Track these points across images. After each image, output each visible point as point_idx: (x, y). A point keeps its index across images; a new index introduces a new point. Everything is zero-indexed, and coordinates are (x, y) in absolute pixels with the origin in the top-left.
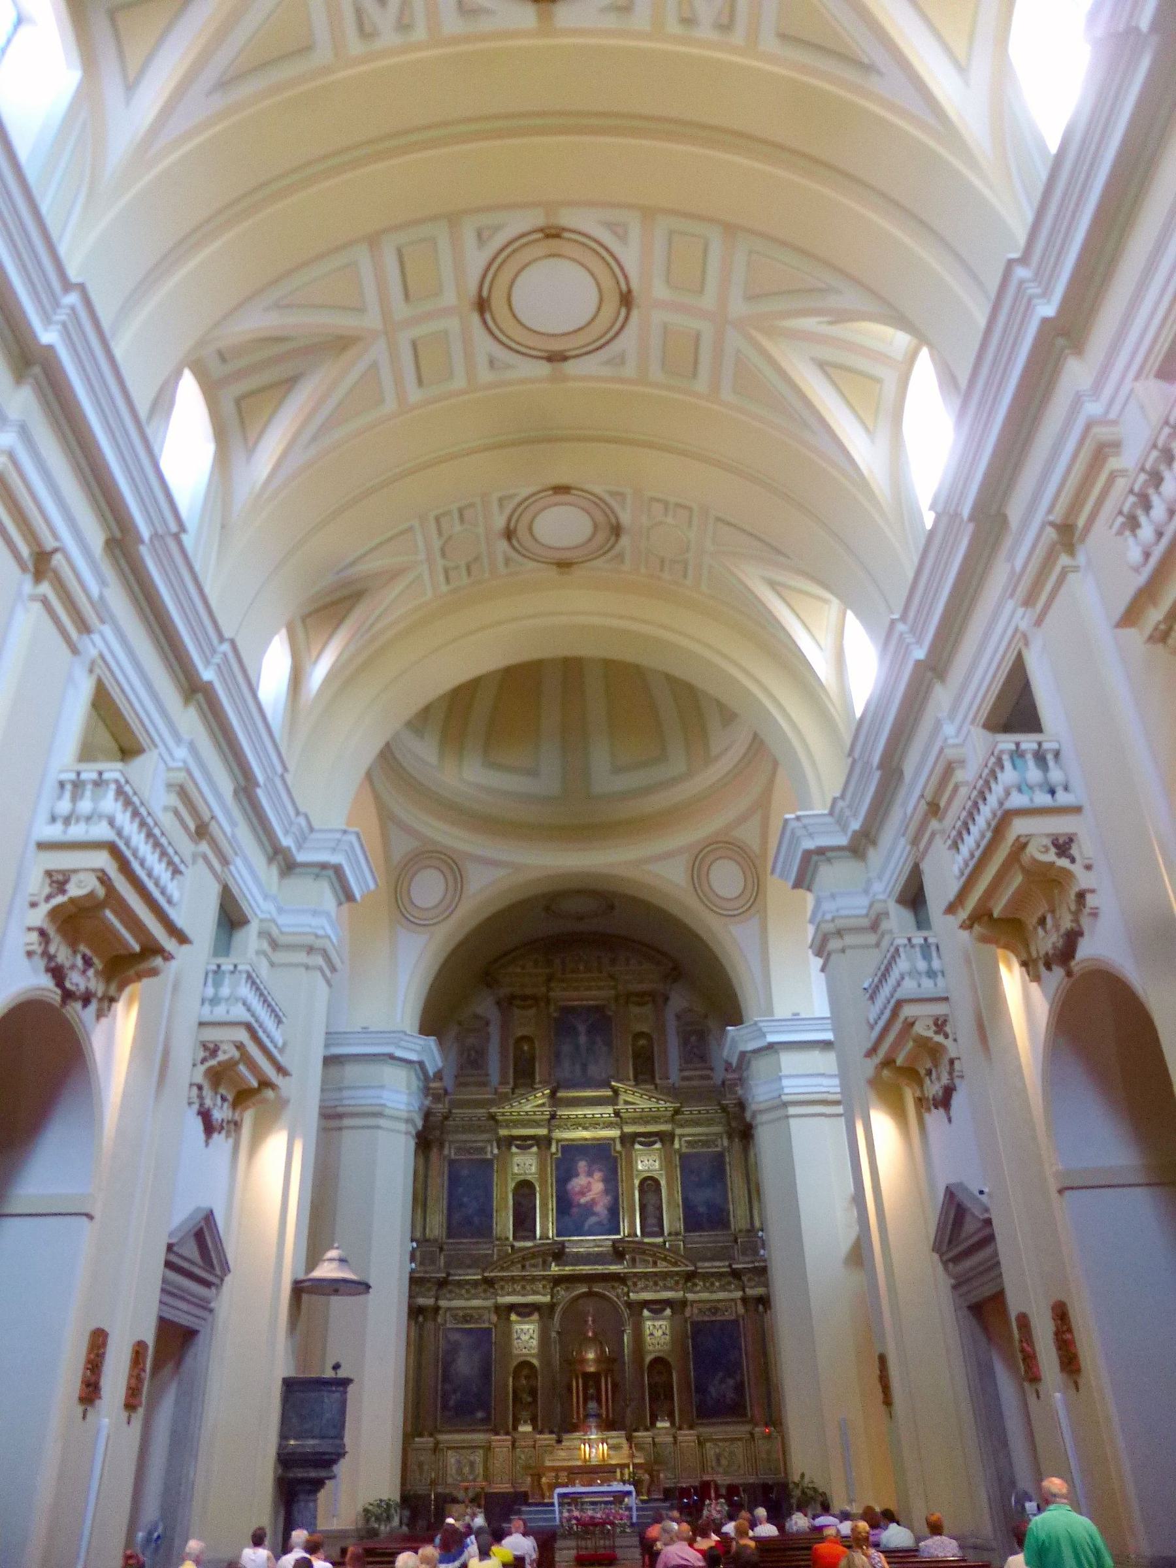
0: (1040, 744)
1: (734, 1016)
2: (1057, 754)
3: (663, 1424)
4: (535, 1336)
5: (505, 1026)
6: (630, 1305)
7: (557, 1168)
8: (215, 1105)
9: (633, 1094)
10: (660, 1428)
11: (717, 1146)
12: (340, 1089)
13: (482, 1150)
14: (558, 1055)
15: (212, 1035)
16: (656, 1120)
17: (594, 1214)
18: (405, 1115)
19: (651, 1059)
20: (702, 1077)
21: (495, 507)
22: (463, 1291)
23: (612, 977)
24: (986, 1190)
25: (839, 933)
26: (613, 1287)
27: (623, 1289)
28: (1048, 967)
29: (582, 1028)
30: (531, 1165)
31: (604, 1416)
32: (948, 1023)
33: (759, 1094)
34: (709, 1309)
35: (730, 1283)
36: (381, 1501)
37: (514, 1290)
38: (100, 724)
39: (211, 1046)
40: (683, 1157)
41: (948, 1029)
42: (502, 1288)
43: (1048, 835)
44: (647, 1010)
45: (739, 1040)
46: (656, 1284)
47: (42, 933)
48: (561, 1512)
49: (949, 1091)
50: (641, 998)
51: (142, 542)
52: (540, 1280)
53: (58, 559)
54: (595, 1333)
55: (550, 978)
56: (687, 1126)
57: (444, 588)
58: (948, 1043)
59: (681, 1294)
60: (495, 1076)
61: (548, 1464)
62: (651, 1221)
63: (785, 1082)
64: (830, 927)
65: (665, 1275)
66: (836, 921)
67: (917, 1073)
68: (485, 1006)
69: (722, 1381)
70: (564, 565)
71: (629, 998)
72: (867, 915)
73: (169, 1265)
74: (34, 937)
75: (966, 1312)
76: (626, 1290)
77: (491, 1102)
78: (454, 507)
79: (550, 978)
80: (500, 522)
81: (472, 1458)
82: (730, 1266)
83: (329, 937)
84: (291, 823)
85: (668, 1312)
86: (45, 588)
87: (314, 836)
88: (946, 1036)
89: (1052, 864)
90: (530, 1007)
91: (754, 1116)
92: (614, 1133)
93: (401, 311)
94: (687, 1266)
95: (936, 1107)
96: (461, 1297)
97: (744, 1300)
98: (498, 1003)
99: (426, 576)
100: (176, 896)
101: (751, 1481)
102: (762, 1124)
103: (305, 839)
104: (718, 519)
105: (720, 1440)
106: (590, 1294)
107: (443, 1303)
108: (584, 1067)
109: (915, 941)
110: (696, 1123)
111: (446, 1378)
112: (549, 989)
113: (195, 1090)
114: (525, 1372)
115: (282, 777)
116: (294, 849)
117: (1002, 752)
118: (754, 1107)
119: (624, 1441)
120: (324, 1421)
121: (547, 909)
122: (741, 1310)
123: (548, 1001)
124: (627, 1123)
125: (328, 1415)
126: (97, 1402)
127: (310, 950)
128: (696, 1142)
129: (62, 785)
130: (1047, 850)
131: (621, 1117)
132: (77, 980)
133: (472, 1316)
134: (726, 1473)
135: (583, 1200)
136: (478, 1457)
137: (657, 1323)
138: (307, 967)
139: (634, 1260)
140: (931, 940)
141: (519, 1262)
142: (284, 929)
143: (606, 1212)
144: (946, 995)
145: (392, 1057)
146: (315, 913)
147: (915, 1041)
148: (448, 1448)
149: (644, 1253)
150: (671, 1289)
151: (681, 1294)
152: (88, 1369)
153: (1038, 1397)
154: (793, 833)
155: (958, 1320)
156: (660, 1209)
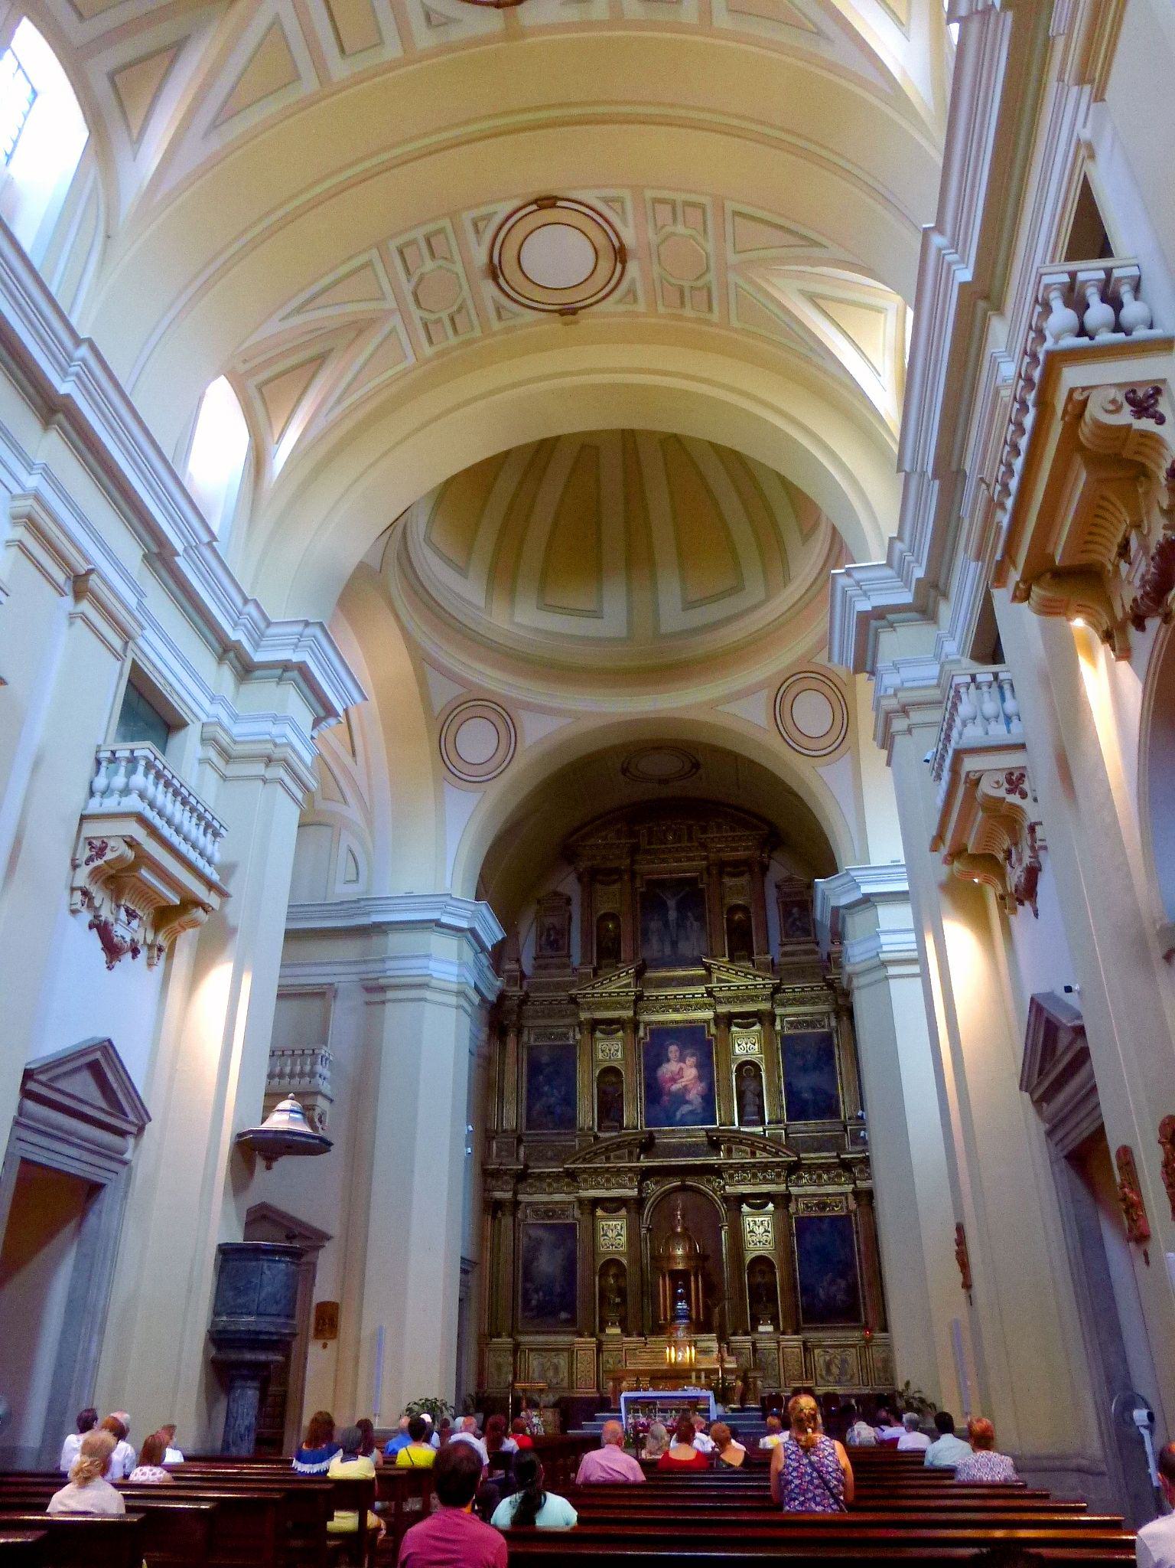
0: (1109, 272)
1: (828, 866)
2: (1137, 288)
3: (766, 1328)
4: (624, 1232)
5: (588, 904)
6: (726, 1199)
7: (646, 1054)
8: (117, 920)
9: (727, 971)
10: (762, 1333)
11: (823, 1027)
12: (383, 960)
13: (565, 1035)
14: (645, 933)
15: (93, 830)
16: (753, 999)
17: (687, 1102)
18: (454, 987)
19: (748, 934)
20: (806, 952)
22: (545, 1185)
23: (703, 846)
24: (1076, 987)
25: (904, 710)
26: (709, 1181)
27: (720, 1183)
28: (1140, 625)
29: (672, 903)
30: (617, 1051)
31: (694, 1317)
32: (1026, 779)
33: (856, 954)
34: (817, 1205)
35: (839, 1176)
36: (427, 1400)
37: (599, 1183)
40: (786, 1039)
41: (1026, 786)
42: (585, 1180)
43: (1119, 386)
44: (743, 881)
45: (830, 892)
46: (755, 1176)
48: (627, 1418)
49: (1033, 874)
50: (738, 867)
51: (178, 555)
52: (625, 1173)
54: (685, 1229)
55: (634, 850)
56: (791, 1005)
57: (428, 351)
58: (1026, 804)
59: (783, 1187)
60: (576, 958)
61: (630, 1367)
62: (750, 1108)
63: (884, 939)
64: (891, 704)
65: (765, 1167)
66: (900, 695)
67: (993, 858)
68: (569, 885)
69: (832, 1282)
70: (568, 312)
71: (724, 868)
72: (938, 686)
73: (26, 1094)
75: (1063, 1162)
76: (722, 1183)
77: (572, 984)
79: (634, 850)
80: (480, 257)
81: (556, 1361)
82: (838, 1156)
85: (771, 1207)
87: (272, 631)
88: (1024, 795)
89: (1129, 426)
90: (614, 882)
91: (850, 980)
92: (708, 1014)
94: (789, 1156)
95: (1022, 903)
96: (543, 1192)
97: (856, 1193)
98: (580, 879)
99: (401, 329)
101: (867, 1392)
102: (858, 988)
103: (262, 635)
104: (736, 213)
105: (830, 1346)
106: (684, 1188)
107: (521, 1197)
108: (674, 944)
109: (979, 678)
110: (802, 1002)
111: (528, 1276)
112: (633, 862)
113: (78, 895)
114: (613, 1271)
115: (209, 544)
116: (247, 645)
117: (1047, 287)
118: (849, 969)
119: (715, 1345)
120: (263, 1294)
121: (625, 771)
122: (853, 1205)
123: (633, 875)
124: (721, 1003)
125: (268, 1289)
127: (269, 760)
128: (799, 1022)
130: (1118, 409)
131: (714, 997)
133: (554, 1212)
134: (838, 1382)
135: (675, 1087)
136: (562, 1361)
137: (758, 1219)
138: (265, 781)
139: (729, 1151)
140: (1002, 676)
141: (602, 1153)
143: (700, 1100)
144: (1020, 741)
145: (438, 924)
146: (275, 719)
147: (985, 809)
148: (531, 1350)
149: (741, 1143)
150: (772, 1182)
151: (783, 1187)
153: (1147, 1262)
154: (845, 593)
155: (1053, 1174)
156: (760, 1095)
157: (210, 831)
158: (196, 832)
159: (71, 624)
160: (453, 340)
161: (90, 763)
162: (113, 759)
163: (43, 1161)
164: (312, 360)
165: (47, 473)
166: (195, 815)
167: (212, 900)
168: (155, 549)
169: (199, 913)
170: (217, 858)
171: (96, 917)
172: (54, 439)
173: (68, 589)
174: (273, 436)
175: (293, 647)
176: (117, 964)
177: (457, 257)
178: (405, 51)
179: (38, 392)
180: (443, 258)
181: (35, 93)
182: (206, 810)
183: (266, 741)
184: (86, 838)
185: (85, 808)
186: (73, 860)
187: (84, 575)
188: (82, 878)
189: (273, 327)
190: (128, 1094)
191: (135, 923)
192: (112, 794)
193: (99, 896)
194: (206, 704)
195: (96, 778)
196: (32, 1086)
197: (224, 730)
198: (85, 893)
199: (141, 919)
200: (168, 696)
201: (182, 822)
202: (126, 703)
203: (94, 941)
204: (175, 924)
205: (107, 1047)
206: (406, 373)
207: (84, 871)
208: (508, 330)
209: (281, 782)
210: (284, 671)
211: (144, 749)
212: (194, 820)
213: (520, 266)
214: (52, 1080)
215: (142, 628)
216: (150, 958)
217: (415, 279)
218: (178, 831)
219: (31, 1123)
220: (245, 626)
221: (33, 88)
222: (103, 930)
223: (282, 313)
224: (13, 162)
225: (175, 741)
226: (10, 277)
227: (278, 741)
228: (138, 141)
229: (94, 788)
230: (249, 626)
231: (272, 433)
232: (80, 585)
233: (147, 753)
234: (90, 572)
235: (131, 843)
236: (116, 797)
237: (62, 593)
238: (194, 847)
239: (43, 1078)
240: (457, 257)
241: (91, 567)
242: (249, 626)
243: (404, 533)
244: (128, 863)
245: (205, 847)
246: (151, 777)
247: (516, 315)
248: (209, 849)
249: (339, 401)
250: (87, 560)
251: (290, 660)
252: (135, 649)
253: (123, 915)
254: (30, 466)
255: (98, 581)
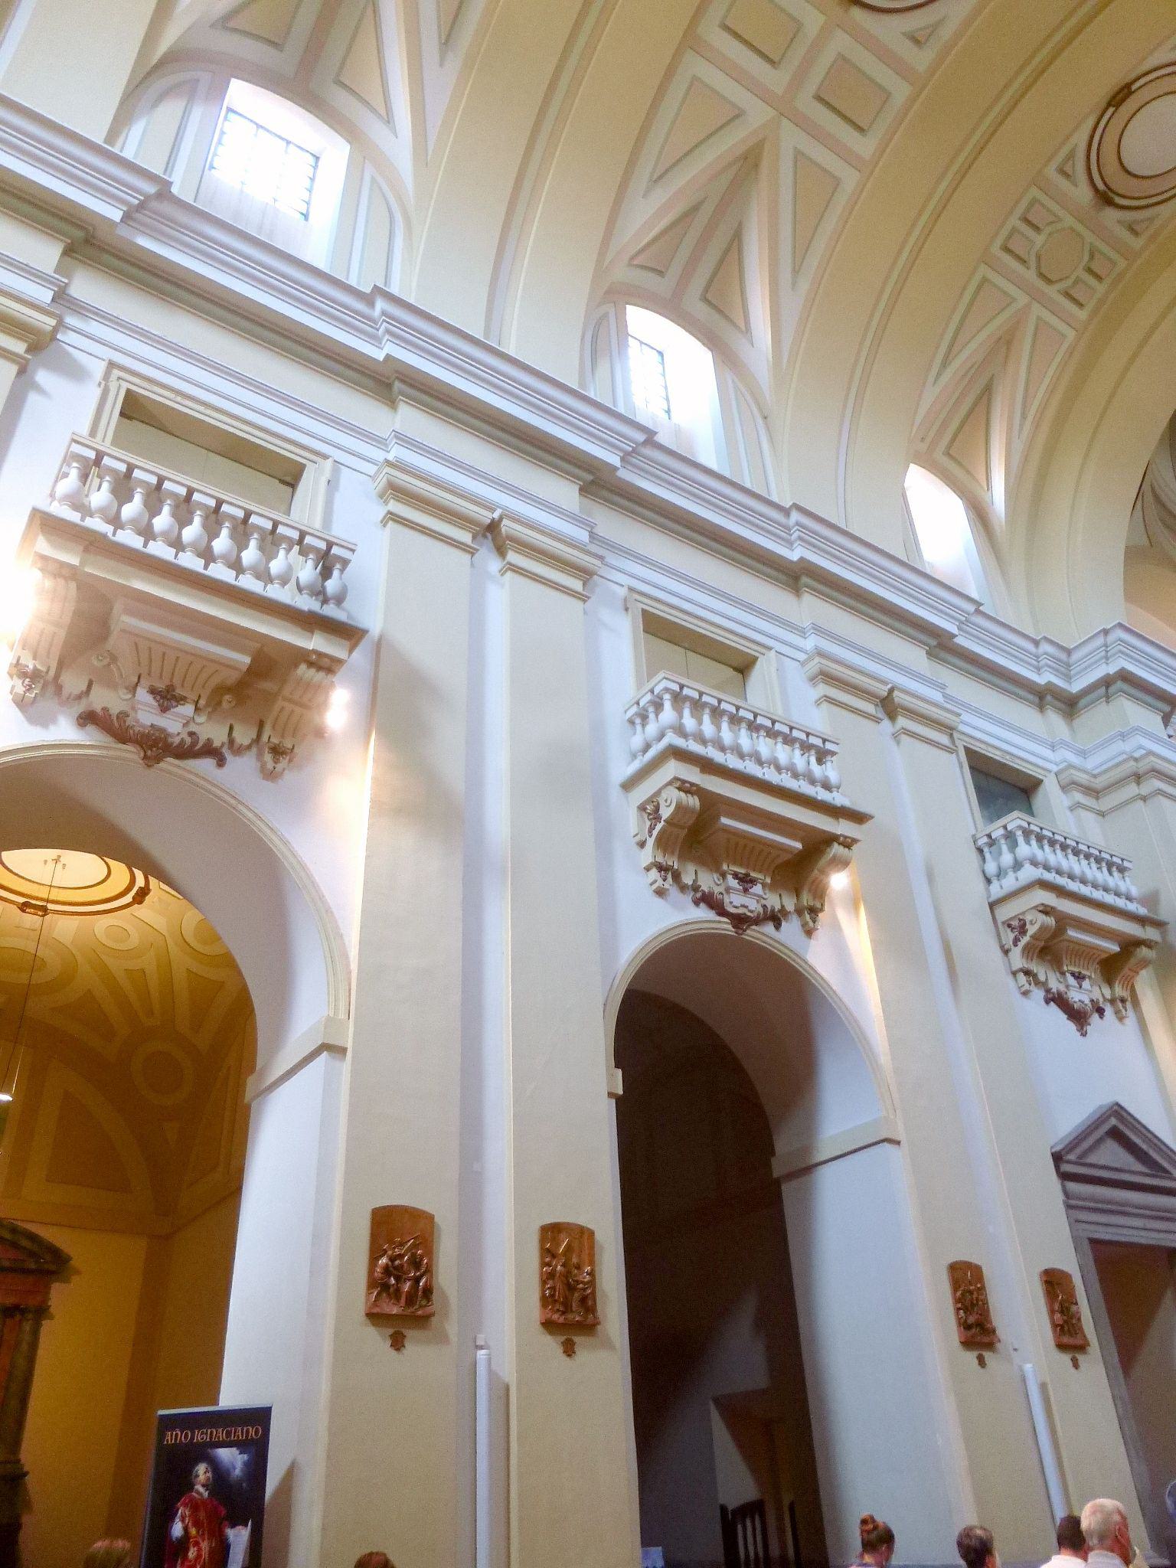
8: (1067, 987)
15: (1006, 912)
21: (1063, 183)
38: (690, 654)
39: (1015, 923)
47: (661, 868)
51: (616, 469)
53: (507, 526)
57: (1082, 315)
73: (1064, 1177)
74: (654, 874)
78: (1014, 221)
80: (1083, 194)
83: (1151, 753)
84: (1038, 657)
86: (512, 557)
87: (1075, 657)
93: (776, 80)
100: (833, 776)
103: (1068, 665)
115: (978, 612)
126: (998, 1345)
127: (1138, 778)
129: (631, 722)
132: (737, 901)
138: (1144, 799)
142: (1095, 772)
146: (1123, 736)
152: (959, 1309)
157: (1114, 869)
158: (1102, 876)
159: (898, 743)
160: (1101, 288)
161: (974, 855)
162: (992, 842)
163: (1107, 1237)
164: (980, 398)
165: (818, 630)
166: (1092, 860)
167: (1150, 933)
168: (933, 642)
169: (1144, 952)
170: (1134, 891)
171: (1048, 991)
172: (809, 600)
173: (881, 714)
174: (982, 487)
175: (1104, 661)
176: (1089, 1029)
177: (1061, 213)
178: (912, 84)
179: (776, 569)
180: (1048, 224)
181: (661, 353)
182: (1100, 852)
183: (1125, 761)
184: (1003, 923)
185: (989, 896)
186: (1002, 947)
187: (886, 697)
188: (1017, 960)
189: (930, 394)
190: (1159, 1150)
191: (1086, 984)
192: (1006, 874)
193: (1041, 971)
194: (1047, 753)
195: (985, 865)
196: (1066, 1168)
197: (1079, 770)
198: (1027, 973)
199: (1090, 977)
200: (1011, 764)
201: (1083, 872)
202: (979, 789)
203: (1055, 1012)
204: (1126, 971)
205: (1117, 1111)
206: (1070, 353)
207: (1016, 953)
208: (1153, 238)
209: (1160, 792)
210: (1107, 687)
211: (1015, 820)
212: (1094, 865)
213: (1136, 176)
214: (1081, 1157)
215: (601, 558)
216: (1117, 1012)
217: (1033, 263)
218: (1084, 881)
219: (1081, 1203)
220: (1049, 667)
221: (311, 153)
222: (1059, 1000)
223: (931, 379)
224: (672, 414)
225: (1038, 800)
226: (706, 493)
227: (1137, 755)
228: (747, 330)
229: (988, 875)
230: (1051, 664)
231: (980, 485)
232: (889, 706)
233: (1019, 822)
234: (891, 691)
235: (1047, 911)
236: (1011, 875)
237: (878, 720)
238: (1106, 890)
239: (1072, 1157)
240: (1061, 213)
241: (889, 686)
242: (1051, 664)
243: (1157, 498)
244: (1052, 931)
245: (1046, 860)
246: (1034, 842)
247: (1151, 220)
248: (1123, 887)
249: (1024, 416)
250: (884, 682)
251: (1108, 674)
252: (962, 737)
253: (1071, 980)
254: (802, 633)
255: (902, 696)
